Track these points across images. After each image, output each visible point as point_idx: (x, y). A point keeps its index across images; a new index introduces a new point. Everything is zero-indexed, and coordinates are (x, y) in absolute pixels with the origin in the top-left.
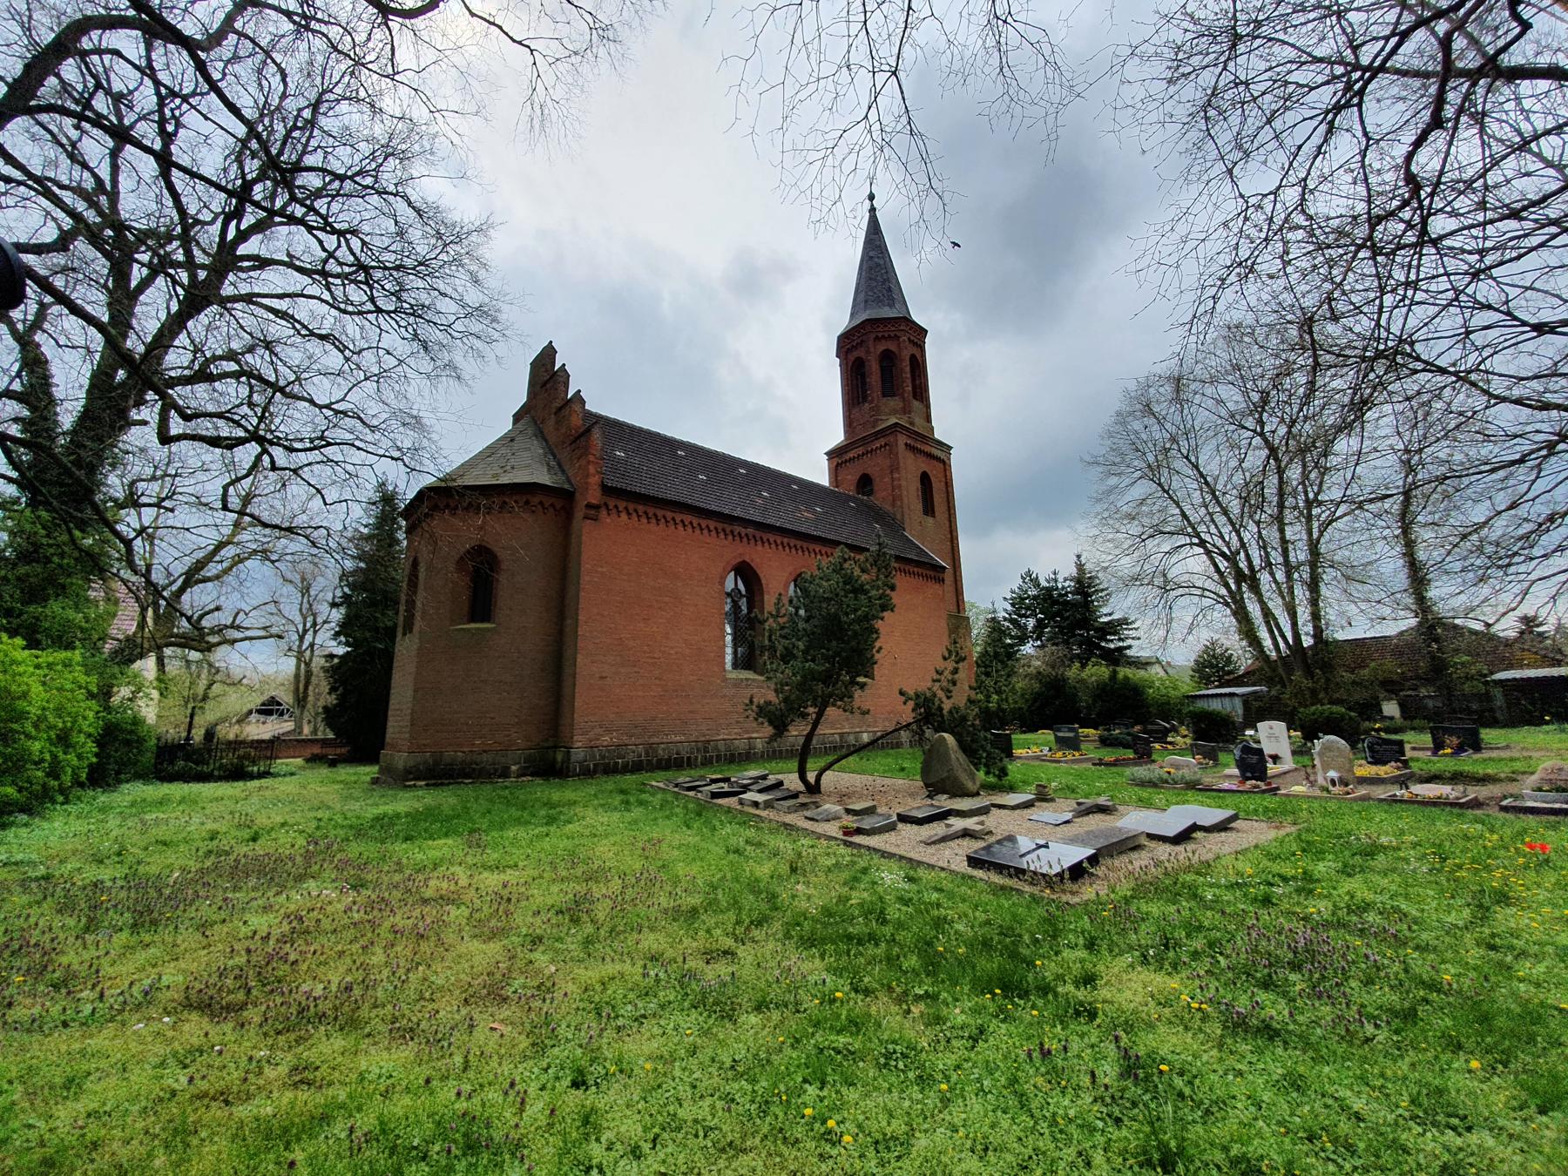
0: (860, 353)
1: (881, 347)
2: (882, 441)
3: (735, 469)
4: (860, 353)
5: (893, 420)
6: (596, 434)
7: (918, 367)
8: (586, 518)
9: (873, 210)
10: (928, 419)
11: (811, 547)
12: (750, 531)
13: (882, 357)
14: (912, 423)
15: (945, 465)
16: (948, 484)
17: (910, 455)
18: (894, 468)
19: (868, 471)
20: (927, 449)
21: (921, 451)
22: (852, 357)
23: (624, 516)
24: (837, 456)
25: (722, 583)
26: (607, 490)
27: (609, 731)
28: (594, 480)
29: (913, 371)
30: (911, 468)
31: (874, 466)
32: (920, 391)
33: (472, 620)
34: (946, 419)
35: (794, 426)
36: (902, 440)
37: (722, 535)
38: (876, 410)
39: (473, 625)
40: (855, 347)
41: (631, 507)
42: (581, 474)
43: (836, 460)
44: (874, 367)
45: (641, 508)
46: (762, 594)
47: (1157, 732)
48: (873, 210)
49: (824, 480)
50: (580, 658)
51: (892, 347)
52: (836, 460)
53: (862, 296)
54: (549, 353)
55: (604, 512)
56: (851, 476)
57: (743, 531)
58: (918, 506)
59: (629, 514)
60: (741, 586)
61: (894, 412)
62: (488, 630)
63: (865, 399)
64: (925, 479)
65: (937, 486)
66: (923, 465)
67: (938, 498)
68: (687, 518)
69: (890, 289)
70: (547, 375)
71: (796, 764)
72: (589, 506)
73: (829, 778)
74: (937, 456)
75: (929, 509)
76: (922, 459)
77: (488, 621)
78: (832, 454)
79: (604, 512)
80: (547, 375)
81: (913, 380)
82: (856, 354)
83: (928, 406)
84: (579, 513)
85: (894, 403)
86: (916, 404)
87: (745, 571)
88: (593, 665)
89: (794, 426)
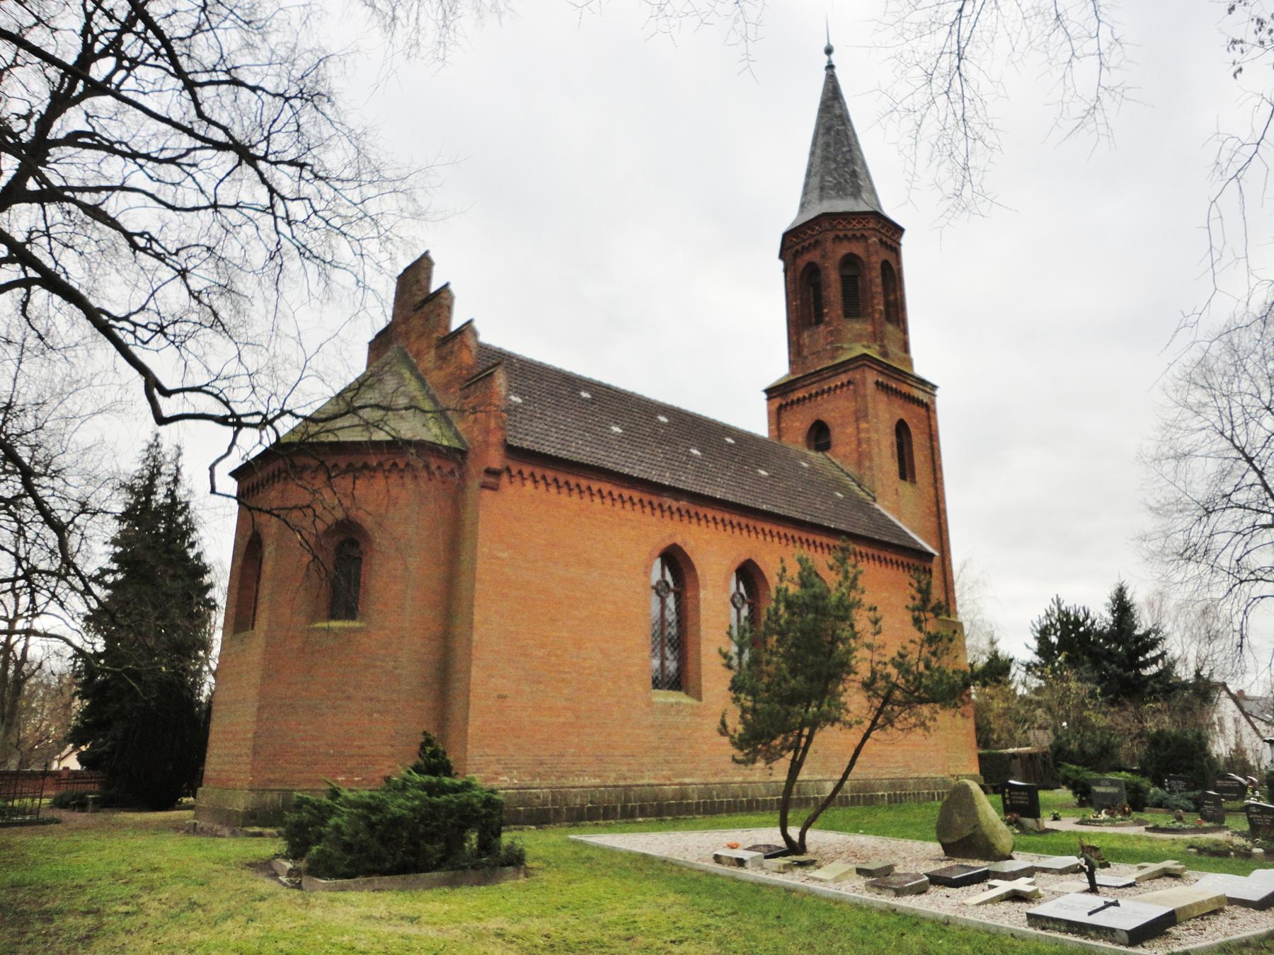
0: (814, 256)
1: (843, 250)
2: (844, 378)
3: (653, 417)
4: (814, 256)
5: (858, 350)
6: (500, 380)
7: (892, 276)
8: (484, 486)
9: (830, 67)
10: (905, 347)
11: (760, 525)
12: (683, 504)
13: (842, 269)
14: (885, 354)
15: (928, 409)
16: (932, 437)
17: (882, 398)
18: (861, 415)
19: (825, 417)
20: (905, 388)
21: (897, 393)
22: (802, 262)
23: (529, 484)
24: (780, 396)
25: (647, 572)
26: (513, 452)
27: (508, 769)
28: (495, 438)
29: (885, 284)
30: (884, 414)
31: (834, 410)
32: (896, 312)
33: (333, 617)
34: (928, 354)
35: (720, 352)
36: (871, 377)
37: (648, 510)
38: (836, 334)
39: (335, 624)
40: (806, 249)
41: (538, 473)
42: (446, 424)
43: (777, 402)
44: (833, 278)
45: (550, 474)
46: (697, 587)
47: (1229, 789)
48: (830, 67)
49: (753, 418)
50: (475, 673)
51: (857, 249)
52: (777, 402)
53: (815, 181)
54: (419, 269)
55: (505, 478)
56: (799, 423)
57: (675, 505)
58: (892, 467)
59: (535, 482)
60: (669, 578)
61: (858, 338)
62: (350, 630)
63: (819, 319)
64: (901, 429)
65: (918, 439)
66: (900, 411)
67: (920, 459)
68: (606, 487)
69: (854, 174)
70: (418, 296)
71: (778, 816)
72: (489, 472)
73: (812, 836)
74: (915, 398)
75: (906, 471)
76: (899, 402)
77: (353, 618)
78: (771, 392)
79: (505, 478)
80: (418, 296)
81: (886, 296)
82: (808, 257)
83: (905, 331)
84: (474, 484)
85: (857, 326)
86: (890, 328)
87: (674, 559)
88: (489, 677)
89: (720, 352)
